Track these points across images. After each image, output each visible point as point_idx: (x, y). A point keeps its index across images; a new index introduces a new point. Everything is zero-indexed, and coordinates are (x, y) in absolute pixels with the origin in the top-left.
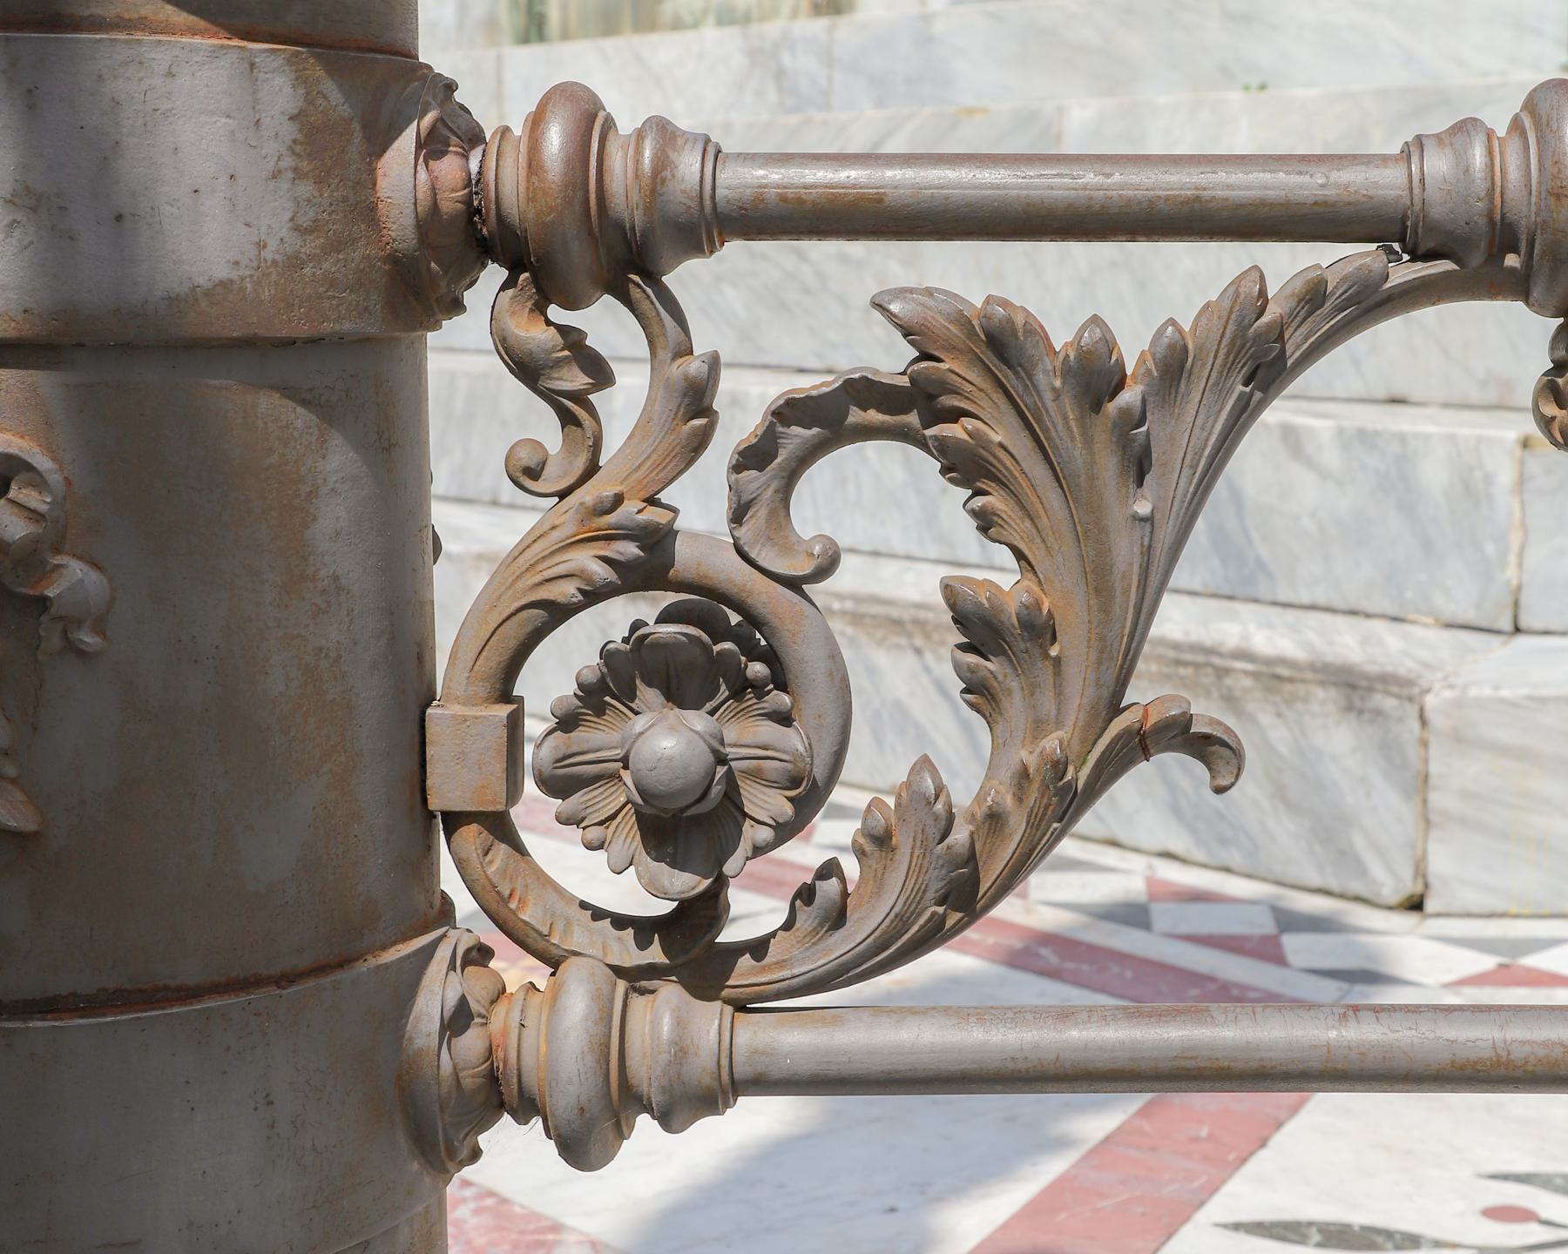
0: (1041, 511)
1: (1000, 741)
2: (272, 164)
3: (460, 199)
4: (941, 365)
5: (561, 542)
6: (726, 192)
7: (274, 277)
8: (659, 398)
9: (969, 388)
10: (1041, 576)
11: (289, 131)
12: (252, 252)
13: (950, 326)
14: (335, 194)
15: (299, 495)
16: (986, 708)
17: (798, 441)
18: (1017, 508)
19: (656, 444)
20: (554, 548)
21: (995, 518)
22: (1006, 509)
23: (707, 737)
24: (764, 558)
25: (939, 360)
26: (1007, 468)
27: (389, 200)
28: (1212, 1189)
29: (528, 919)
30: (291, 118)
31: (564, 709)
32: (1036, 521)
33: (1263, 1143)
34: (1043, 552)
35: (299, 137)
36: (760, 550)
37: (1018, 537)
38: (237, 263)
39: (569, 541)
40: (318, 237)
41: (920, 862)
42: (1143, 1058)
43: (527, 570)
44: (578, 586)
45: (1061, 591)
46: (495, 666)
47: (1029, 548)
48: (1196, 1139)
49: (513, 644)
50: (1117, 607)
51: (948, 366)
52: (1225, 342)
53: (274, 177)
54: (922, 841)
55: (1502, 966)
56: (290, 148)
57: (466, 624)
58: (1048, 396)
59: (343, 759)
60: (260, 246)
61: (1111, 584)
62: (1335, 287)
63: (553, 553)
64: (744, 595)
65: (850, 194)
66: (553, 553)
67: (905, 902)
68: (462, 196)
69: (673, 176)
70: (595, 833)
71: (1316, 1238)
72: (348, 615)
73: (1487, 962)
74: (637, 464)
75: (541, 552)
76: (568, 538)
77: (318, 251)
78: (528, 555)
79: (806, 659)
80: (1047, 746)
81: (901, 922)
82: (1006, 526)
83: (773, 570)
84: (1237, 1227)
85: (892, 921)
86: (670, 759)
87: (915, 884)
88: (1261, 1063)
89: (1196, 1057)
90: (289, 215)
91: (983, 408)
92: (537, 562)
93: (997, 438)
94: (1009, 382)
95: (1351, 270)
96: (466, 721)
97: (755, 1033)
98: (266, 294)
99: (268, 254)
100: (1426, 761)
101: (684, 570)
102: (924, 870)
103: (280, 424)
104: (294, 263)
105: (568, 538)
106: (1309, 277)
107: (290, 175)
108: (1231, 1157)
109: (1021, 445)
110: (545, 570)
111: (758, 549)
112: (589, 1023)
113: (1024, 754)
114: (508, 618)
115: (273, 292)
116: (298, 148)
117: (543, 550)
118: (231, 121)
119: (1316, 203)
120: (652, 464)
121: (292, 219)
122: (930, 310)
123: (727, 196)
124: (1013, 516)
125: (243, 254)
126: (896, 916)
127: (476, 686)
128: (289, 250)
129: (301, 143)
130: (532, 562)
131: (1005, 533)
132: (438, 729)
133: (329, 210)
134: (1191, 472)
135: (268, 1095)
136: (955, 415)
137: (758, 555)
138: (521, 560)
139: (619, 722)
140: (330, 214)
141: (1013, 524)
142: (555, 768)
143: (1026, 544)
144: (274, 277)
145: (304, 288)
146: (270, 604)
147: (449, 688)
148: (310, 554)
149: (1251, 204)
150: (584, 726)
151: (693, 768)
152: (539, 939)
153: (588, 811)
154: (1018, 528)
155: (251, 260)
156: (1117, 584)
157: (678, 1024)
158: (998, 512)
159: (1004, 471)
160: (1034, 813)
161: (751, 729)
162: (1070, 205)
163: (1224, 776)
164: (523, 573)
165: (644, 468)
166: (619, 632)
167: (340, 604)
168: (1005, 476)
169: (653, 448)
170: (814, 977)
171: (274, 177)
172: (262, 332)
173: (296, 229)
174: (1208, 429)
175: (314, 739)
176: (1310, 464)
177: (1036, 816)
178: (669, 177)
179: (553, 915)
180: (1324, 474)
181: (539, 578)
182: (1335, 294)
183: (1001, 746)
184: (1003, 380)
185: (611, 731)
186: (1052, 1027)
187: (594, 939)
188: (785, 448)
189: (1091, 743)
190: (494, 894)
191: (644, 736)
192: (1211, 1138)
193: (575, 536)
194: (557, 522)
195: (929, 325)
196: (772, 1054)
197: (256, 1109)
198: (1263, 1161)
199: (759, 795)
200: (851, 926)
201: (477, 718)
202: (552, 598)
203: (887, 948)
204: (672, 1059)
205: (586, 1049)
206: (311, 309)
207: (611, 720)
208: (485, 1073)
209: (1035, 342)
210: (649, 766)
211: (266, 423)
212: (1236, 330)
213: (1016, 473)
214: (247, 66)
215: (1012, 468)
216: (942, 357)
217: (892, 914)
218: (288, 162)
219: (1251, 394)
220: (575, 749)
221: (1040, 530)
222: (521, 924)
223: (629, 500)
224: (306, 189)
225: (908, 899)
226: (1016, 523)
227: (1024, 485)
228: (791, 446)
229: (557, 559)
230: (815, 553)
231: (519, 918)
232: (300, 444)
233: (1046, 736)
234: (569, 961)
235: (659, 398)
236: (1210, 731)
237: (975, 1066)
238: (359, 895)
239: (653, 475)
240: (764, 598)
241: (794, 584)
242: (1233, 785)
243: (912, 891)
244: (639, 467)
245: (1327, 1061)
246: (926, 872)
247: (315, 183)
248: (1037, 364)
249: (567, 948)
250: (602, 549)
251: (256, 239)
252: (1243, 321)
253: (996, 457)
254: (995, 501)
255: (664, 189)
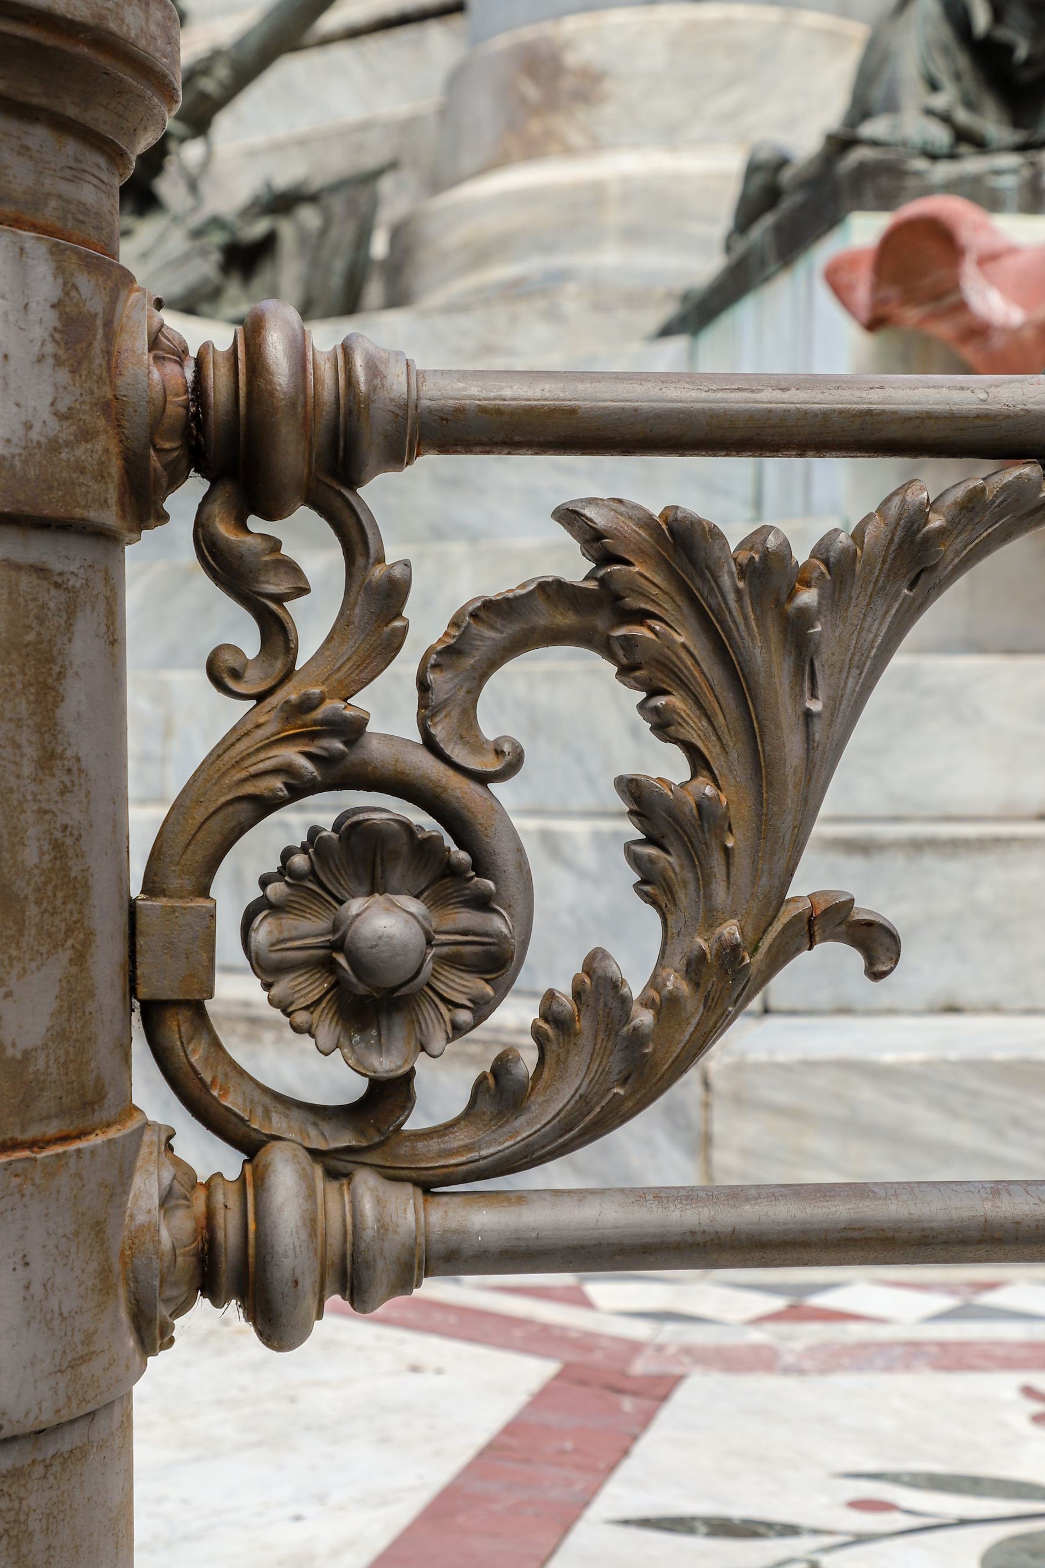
0: (718, 711)
1: (674, 931)
2: (37, 348)
3: (181, 403)
4: (631, 568)
5: (266, 739)
6: (428, 403)
7: (38, 457)
8: (360, 602)
9: (655, 591)
10: (716, 772)
11: (51, 319)
12: (20, 431)
13: (640, 531)
14: (84, 385)
15: (51, 675)
16: (663, 900)
17: (488, 643)
18: (694, 707)
19: (357, 645)
20: (259, 745)
21: (676, 717)
22: (685, 708)
23: (420, 918)
24: (457, 756)
25: (629, 563)
26: (687, 668)
27: (125, 399)
28: (592, 1493)
29: (230, 1106)
30: (53, 306)
31: (278, 896)
32: (713, 720)
33: (625, 1453)
34: (718, 749)
35: (58, 324)
36: (454, 748)
37: (695, 735)
38: (8, 441)
39: (274, 738)
40: (71, 425)
41: (604, 1045)
42: (814, 1229)
43: (233, 766)
44: (285, 781)
45: (735, 786)
46: (201, 859)
47: (706, 746)
48: (563, 1452)
49: (217, 838)
50: (789, 800)
51: (637, 569)
52: (893, 548)
53: (39, 361)
54: (607, 1025)
55: (792, 1307)
56: (52, 336)
57: (170, 821)
58: (731, 597)
59: (82, 936)
60: (28, 426)
61: (784, 777)
62: (996, 496)
63: (258, 750)
64: (439, 790)
65: (546, 405)
66: (258, 750)
67: (589, 1084)
68: (183, 400)
69: (383, 385)
70: (301, 1017)
71: (703, 1529)
72: (86, 796)
73: (778, 1303)
74: (338, 664)
75: (246, 750)
76: (273, 735)
77: (72, 438)
78: (234, 752)
79: (497, 852)
80: (725, 932)
81: (584, 1102)
82: (684, 724)
83: (467, 766)
84: (626, 1522)
85: (576, 1102)
86: (390, 937)
87: (599, 1066)
88: (923, 1233)
89: (864, 1228)
90: (49, 400)
91: (667, 610)
92: (243, 759)
93: (680, 639)
94: (694, 584)
95: (1010, 479)
96: (174, 911)
97: (446, 1212)
98: (32, 473)
99: (35, 435)
100: (708, 1121)
101: (383, 766)
102: (608, 1052)
103: (38, 603)
104: (54, 446)
105: (273, 735)
106: (972, 486)
107: (50, 361)
108: (602, 1465)
109: (700, 649)
110: (250, 766)
111: (451, 746)
112: (301, 1200)
113: (700, 941)
114: (214, 813)
115: (37, 471)
116: (58, 336)
117: (249, 748)
118: (5, 302)
119: (978, 417)
120: (353, 665)
121: (52, 404)
122: (622, 515)
123: (429, 407)
124: (691, 714)
125: (13, 432)
126: (581, 1096)
127: (182, 879)
128: (51, 434)
129: (60, 332)
130: (238, 759)
131: (683, 731)
132: (147, 919)
133: (80, 399)
134: (858, 672)
135: (25, 1256)
136: (641, 617)
137: (452, 752)
138: (226, 757)
139: (325, 912)
140: (81, 403)
141: (691, 722)
142: (270, 951)
143: (703, 742)
144: (38, 457)
145: (61, 472)
146: (28, 777)
147: (154, 882)
148: (59, 733)
149: (917, 418)
150: (292, 913)
151: (411, 946)
152: (240, 1124)
153: (296, 996)
154: (695, 730)
155: (20, 440)
156: (789, 778)
157: (378, 1202)
158: (678, 710)
159: (685, 671)
160: (711, 996)
161: (450, 916)
162: (751, 417)
163: (883, 963)
164: (228, 769)
165: (345, 669)
166: (326, 820)
167: (80, 785)
168: (686, 677)
169: (353, 649)
170: (500, 1159)
171: (39, 361)
172: (27, 510)
173: (56, 414)
174: (874, 631)
175: (61, 913)
176: (568, 865)
177: (713, 999)
178: (379, 386)
179: (252, 1102)
180: (581, 873)
181: (244, 774)
182: (994, 502)
183: (675, 936)
184: (689, 582)
185: (316, 920)
186: (725, 1202)
187: (291, 1124)
188: (478, 649)
189: (762, 930)
190: (197, 1081)
191: (360, 917)
192: (576, 1450)
193: (279, 733)
194: (261, 720)
195: (621, 529)
196: (464, 1232)
197: (14, 1269)
198: (628, 1467)
199: (457, 980)
200: (536, 1109)
201: (185, 908)
202: (258, 793)
203: (571, 1130)
204: (376, 1235)
205: (300, 1224)
206: (67, 493)
207: (316, 909)
208: (194, 1252)
209: (721, 545)
210: (369, 944)
211: (26, 601)
212: (905, 535)
213: (696, 674)
214: (18, 250)
215: (692, 668)
216: (632, 560)
217: (577, 1096)
218: (50, 348)
219: (914, 599)
220: (285, 935)
221: (717, 727)
222: (223, 1111)
223: (330, 699)
224: (63, 376)
225: (592, 1079)
226: (694, 722)
227: (703, 685)
228: (483, 648)
229: (262, 755)
230: (505, 750)
231: (220, 1104)
232: (53, 625)
233: (721, 924)
234: (269, 1145)
235: (360, 602)
236: (873, 919)
237: (656, 1240)
238: (92, 1071)
239: (354, 675)
240: (458, 793)
241: (483, 779)
242: (892, 970)
243: (596, 1072)
244: (340, 668)
245: (985, 1230)
246: (611, 1054)
247: (70, 372)
248: (723, 566)
249: (267, 1132)
250: (306, 745)
251: (24, 419)
252: (912, 526)
253: (679, 657)
254: (675, 701)
255: (375, 397)
